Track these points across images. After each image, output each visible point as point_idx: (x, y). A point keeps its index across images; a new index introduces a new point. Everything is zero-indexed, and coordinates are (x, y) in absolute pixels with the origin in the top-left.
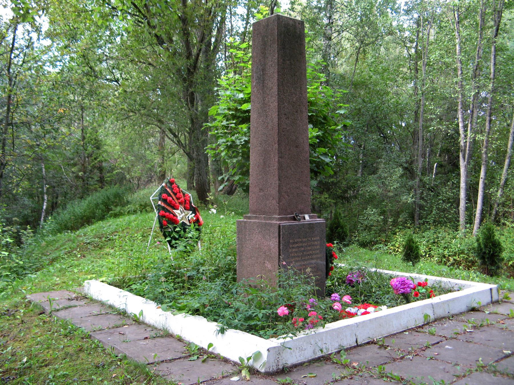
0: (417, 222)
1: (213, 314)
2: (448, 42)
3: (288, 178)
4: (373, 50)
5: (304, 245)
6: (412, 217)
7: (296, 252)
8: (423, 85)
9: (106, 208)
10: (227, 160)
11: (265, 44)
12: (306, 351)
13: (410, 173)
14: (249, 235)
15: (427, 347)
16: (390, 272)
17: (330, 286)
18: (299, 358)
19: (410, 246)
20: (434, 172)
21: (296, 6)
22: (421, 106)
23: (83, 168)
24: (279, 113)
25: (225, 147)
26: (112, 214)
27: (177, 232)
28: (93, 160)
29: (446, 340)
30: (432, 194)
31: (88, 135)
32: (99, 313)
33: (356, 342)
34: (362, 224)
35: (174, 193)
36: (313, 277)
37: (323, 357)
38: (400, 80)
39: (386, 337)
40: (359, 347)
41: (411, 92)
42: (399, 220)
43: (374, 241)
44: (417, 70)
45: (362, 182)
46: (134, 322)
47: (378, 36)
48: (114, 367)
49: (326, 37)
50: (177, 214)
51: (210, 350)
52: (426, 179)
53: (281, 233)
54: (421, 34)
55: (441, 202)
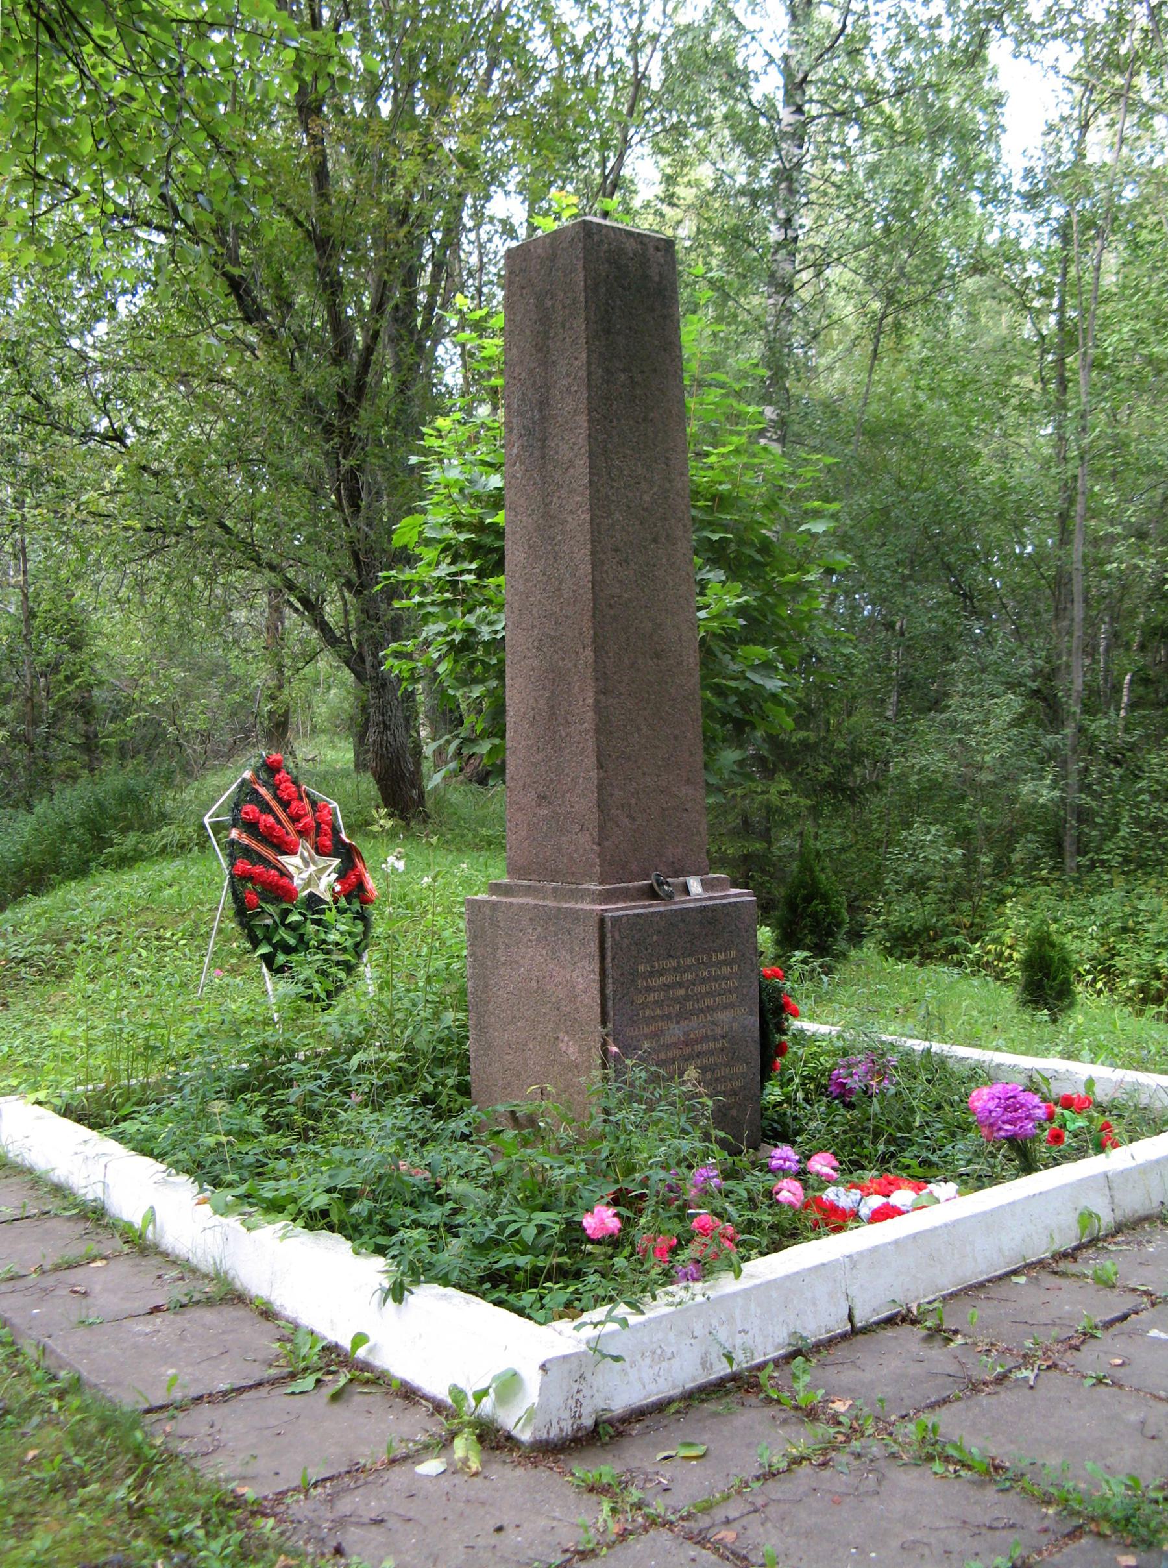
0: (1070, 863)
1: (374, 1228)
2: (1160, 293)
3: (629, 759)
4: (927, 321)
5: (685, 977)
6: (1056, 845)
7: (659, 1004)
8: (1084, 429)
9: (95, 838)
10: (451, 692)
11: (544, 319)
12: (676, 1363)
13: (1049, 706)
14: (508, 946)
15: (1087, 1336)
16: (974, 1054)
17: (780, 1104)
18: (652, 1387)
19: (1042, 958)
20: (1125, 699)
21: (680, 191)
22: (1080, 498)
23: (28, 709)
24: (593, 546)
25: (445, 648)
26: (111, 855)
27: (293, 927)
28: (60, 682)
29: (1153, 1305)
30: (1117, 772)
31: (45, 606)
32: (19, 1213)
33: (851, 1318)
34: (897, 874)
35: (280, 800)
36: (705, 1100)
37: (734, 1377)
38: (1012, 416)
39: (952, 1295)
40: (860, 1337)
41: (1047, 451)
42: (1015, 857)
43: (934, 928)
44: (1063, 384)
45: (896, 740)
46: (126, 1248)
47: (941, 277)
48: (36, 1419)
49: (777, 285)
50: (292, 869)
51: (361, 1353)
52: (1098, 726)
53: (609, 943)
54: (1073, 271)
55: (1146, 797)
